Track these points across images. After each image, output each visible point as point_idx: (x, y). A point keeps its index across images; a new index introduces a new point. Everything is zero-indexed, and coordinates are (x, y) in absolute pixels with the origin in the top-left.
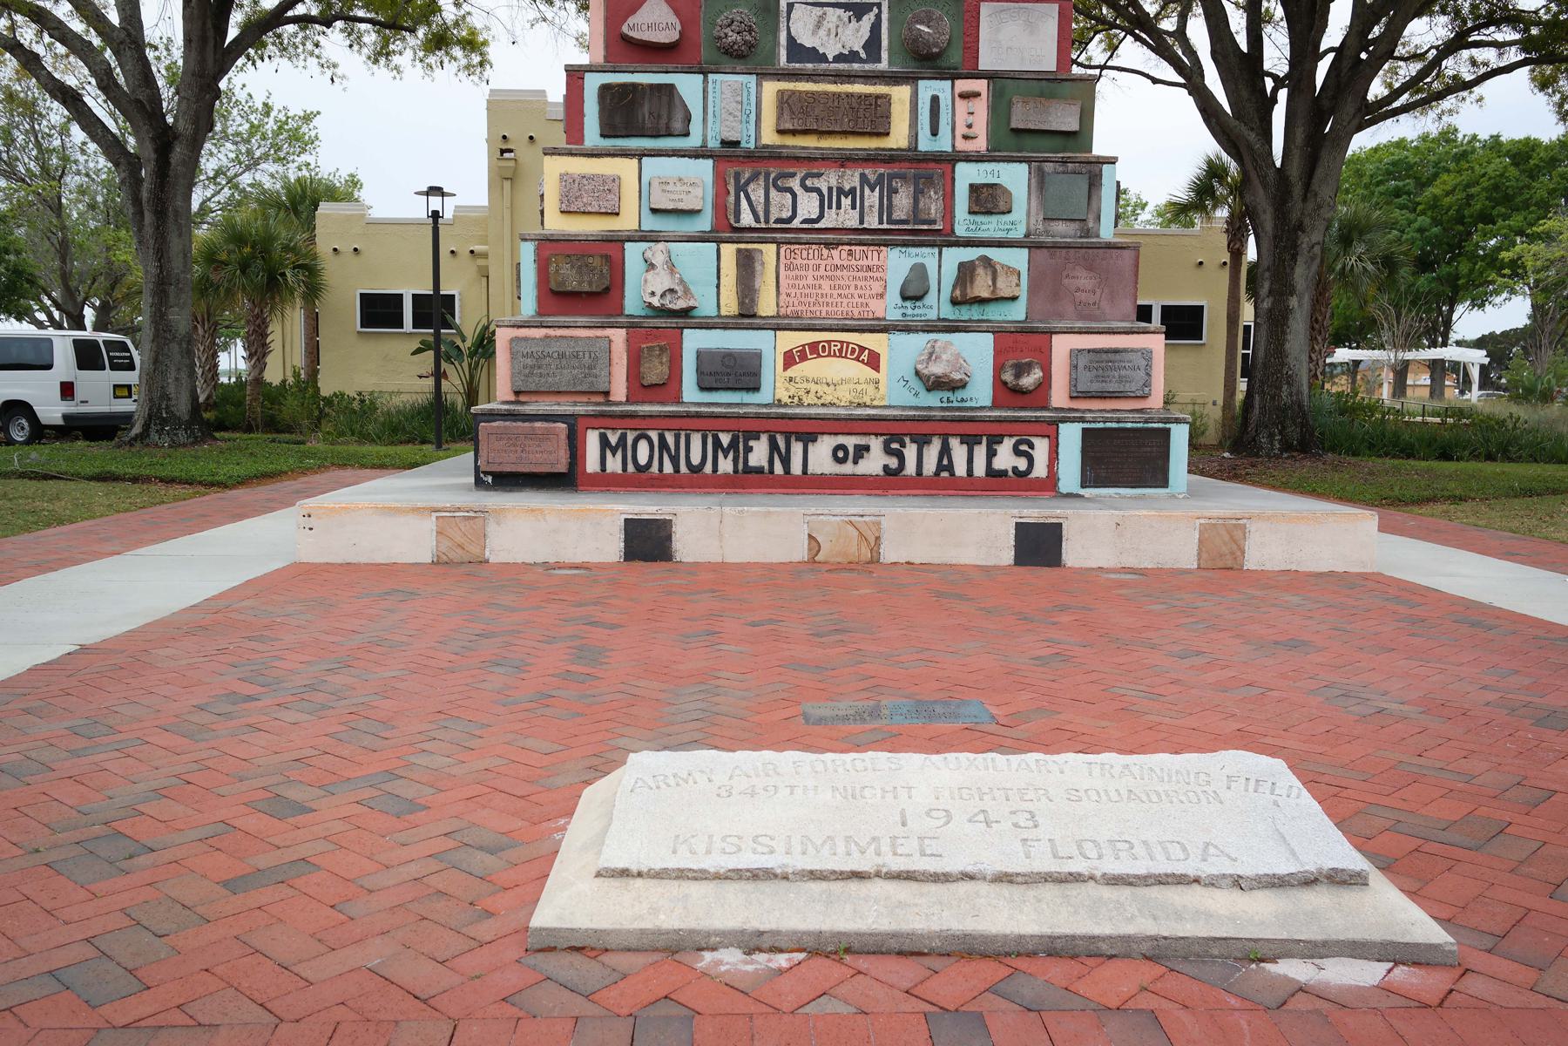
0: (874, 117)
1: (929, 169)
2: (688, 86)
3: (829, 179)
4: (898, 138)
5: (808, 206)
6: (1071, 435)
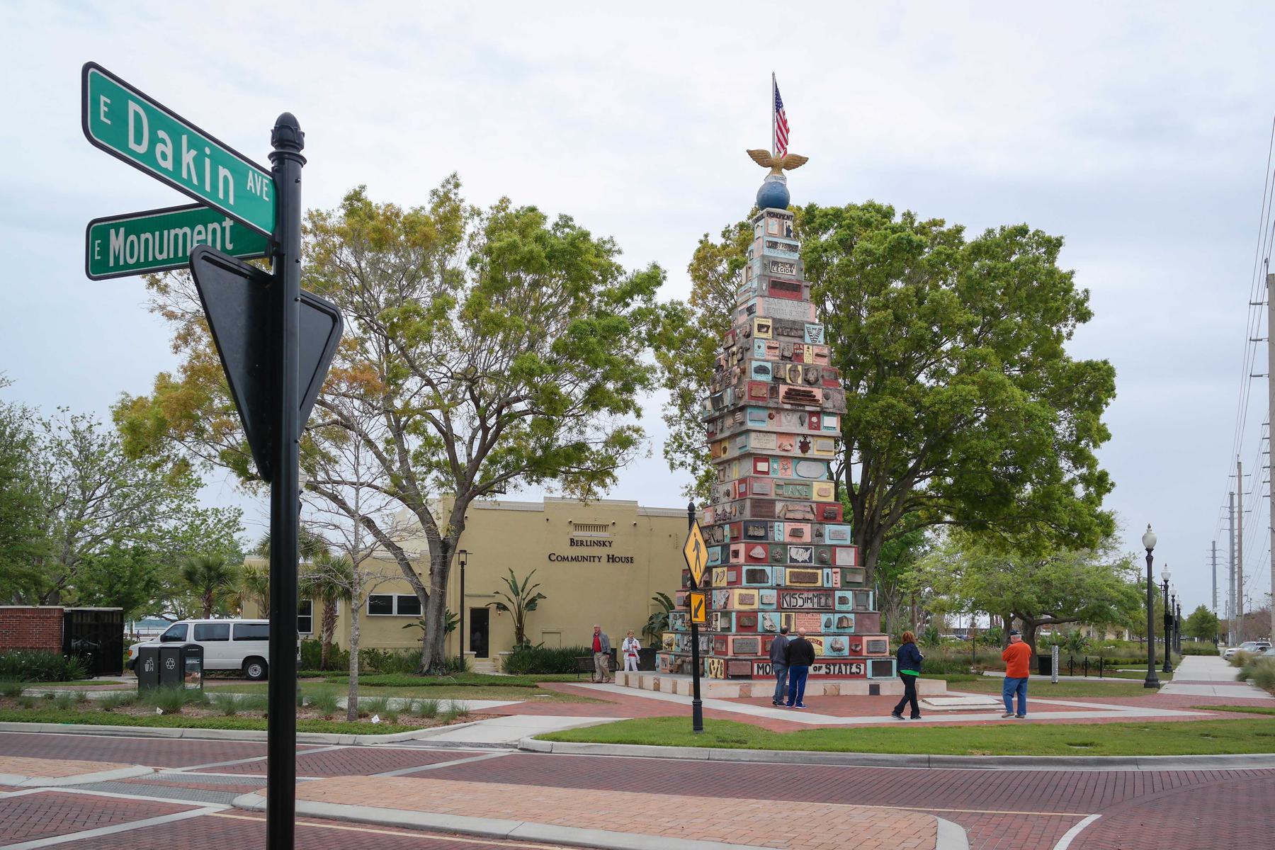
0: (813, 578)
1: (829, 592)
2: (768, 569)
3: (805, 595)
4: (819, 584)
5: (800, 602)
6: (869, 663)
